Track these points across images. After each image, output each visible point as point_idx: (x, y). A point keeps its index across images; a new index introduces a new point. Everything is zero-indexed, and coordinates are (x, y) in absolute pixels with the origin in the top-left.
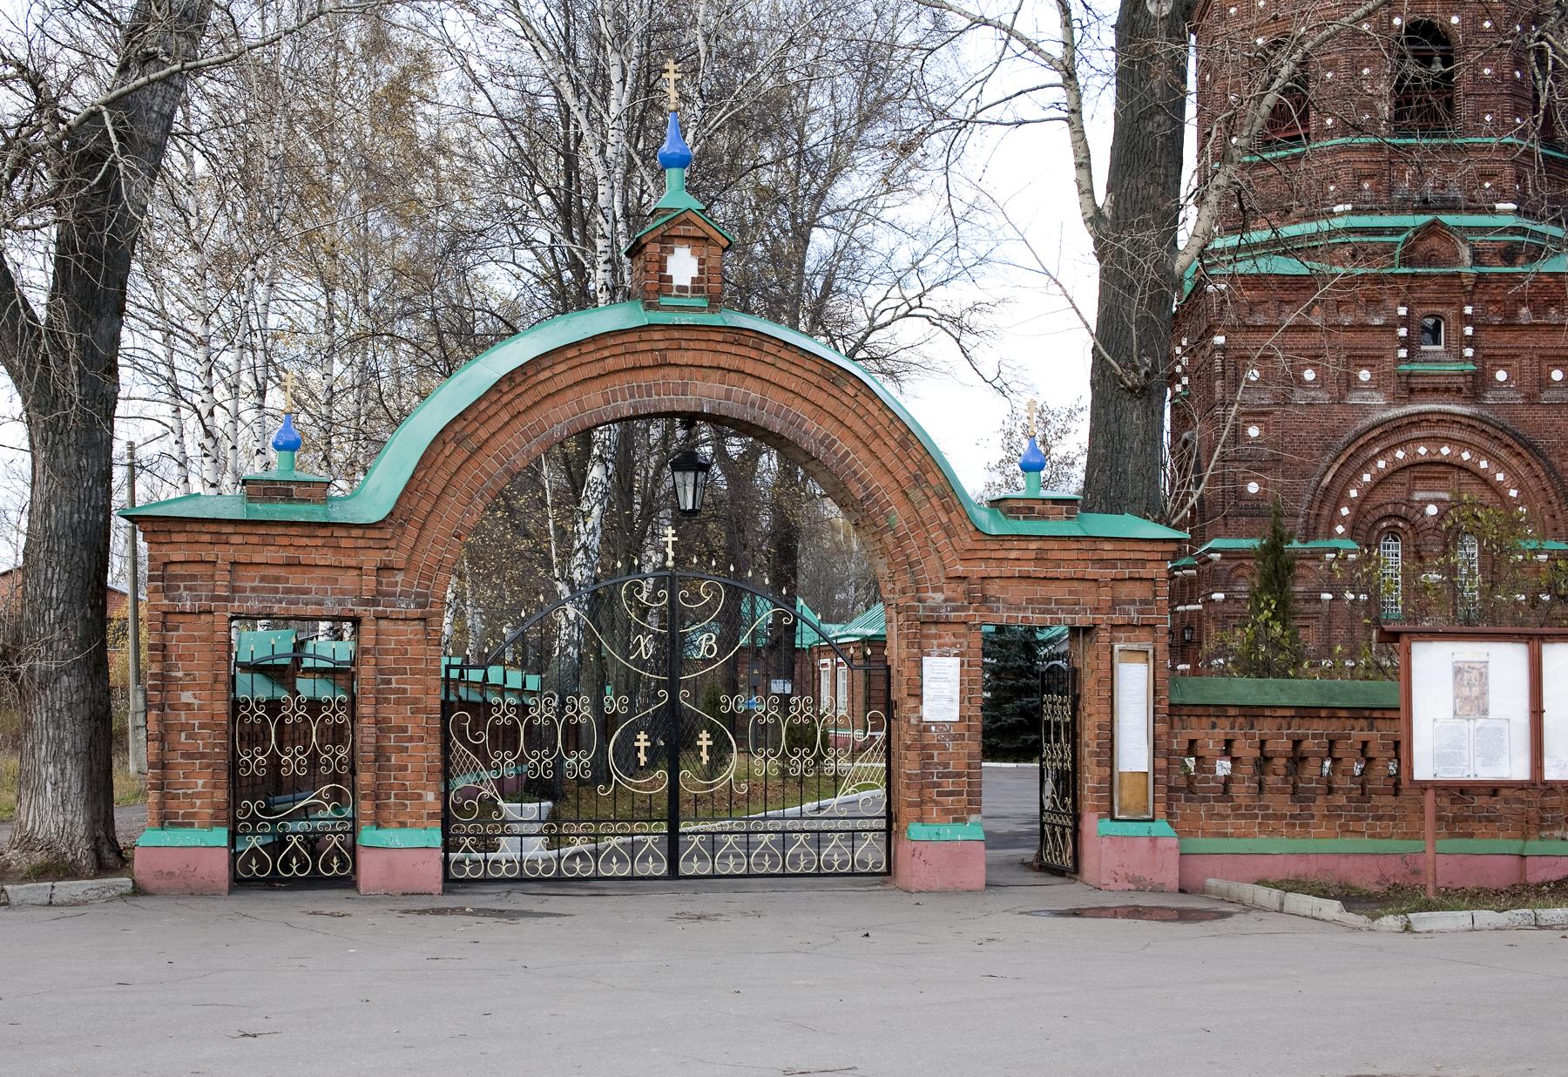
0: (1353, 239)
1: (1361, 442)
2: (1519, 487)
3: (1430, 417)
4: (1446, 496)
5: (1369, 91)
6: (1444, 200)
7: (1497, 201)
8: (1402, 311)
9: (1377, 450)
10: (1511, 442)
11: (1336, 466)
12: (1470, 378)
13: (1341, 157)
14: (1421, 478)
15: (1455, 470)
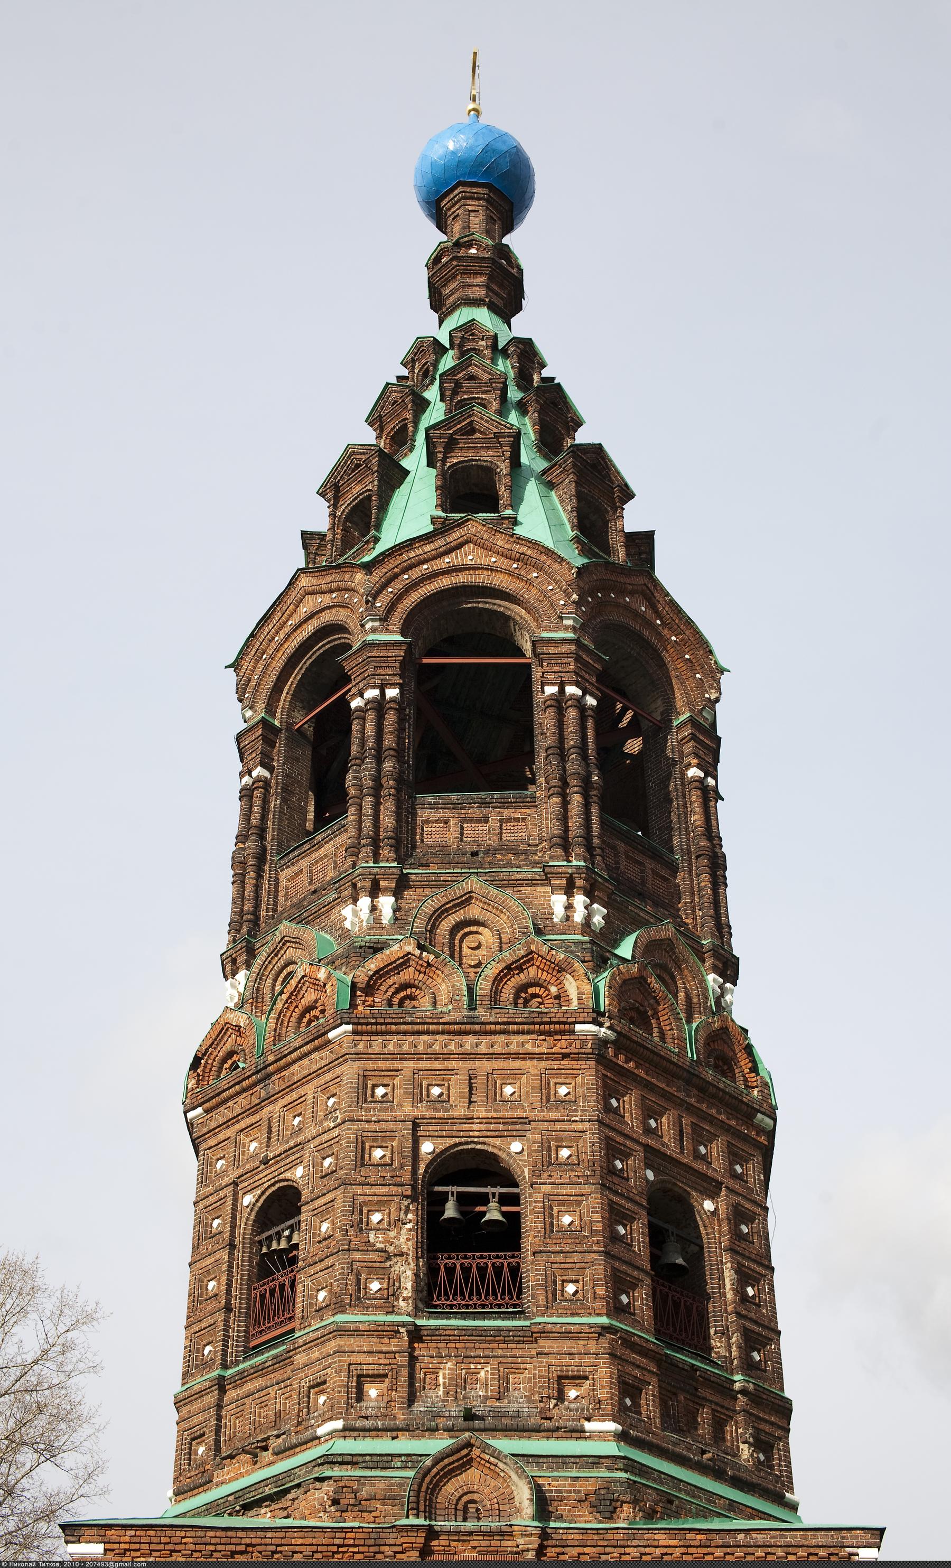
0: (337, 1472)
5: (379, 1246)
6: (500, 1415)
13: (332, 1345)
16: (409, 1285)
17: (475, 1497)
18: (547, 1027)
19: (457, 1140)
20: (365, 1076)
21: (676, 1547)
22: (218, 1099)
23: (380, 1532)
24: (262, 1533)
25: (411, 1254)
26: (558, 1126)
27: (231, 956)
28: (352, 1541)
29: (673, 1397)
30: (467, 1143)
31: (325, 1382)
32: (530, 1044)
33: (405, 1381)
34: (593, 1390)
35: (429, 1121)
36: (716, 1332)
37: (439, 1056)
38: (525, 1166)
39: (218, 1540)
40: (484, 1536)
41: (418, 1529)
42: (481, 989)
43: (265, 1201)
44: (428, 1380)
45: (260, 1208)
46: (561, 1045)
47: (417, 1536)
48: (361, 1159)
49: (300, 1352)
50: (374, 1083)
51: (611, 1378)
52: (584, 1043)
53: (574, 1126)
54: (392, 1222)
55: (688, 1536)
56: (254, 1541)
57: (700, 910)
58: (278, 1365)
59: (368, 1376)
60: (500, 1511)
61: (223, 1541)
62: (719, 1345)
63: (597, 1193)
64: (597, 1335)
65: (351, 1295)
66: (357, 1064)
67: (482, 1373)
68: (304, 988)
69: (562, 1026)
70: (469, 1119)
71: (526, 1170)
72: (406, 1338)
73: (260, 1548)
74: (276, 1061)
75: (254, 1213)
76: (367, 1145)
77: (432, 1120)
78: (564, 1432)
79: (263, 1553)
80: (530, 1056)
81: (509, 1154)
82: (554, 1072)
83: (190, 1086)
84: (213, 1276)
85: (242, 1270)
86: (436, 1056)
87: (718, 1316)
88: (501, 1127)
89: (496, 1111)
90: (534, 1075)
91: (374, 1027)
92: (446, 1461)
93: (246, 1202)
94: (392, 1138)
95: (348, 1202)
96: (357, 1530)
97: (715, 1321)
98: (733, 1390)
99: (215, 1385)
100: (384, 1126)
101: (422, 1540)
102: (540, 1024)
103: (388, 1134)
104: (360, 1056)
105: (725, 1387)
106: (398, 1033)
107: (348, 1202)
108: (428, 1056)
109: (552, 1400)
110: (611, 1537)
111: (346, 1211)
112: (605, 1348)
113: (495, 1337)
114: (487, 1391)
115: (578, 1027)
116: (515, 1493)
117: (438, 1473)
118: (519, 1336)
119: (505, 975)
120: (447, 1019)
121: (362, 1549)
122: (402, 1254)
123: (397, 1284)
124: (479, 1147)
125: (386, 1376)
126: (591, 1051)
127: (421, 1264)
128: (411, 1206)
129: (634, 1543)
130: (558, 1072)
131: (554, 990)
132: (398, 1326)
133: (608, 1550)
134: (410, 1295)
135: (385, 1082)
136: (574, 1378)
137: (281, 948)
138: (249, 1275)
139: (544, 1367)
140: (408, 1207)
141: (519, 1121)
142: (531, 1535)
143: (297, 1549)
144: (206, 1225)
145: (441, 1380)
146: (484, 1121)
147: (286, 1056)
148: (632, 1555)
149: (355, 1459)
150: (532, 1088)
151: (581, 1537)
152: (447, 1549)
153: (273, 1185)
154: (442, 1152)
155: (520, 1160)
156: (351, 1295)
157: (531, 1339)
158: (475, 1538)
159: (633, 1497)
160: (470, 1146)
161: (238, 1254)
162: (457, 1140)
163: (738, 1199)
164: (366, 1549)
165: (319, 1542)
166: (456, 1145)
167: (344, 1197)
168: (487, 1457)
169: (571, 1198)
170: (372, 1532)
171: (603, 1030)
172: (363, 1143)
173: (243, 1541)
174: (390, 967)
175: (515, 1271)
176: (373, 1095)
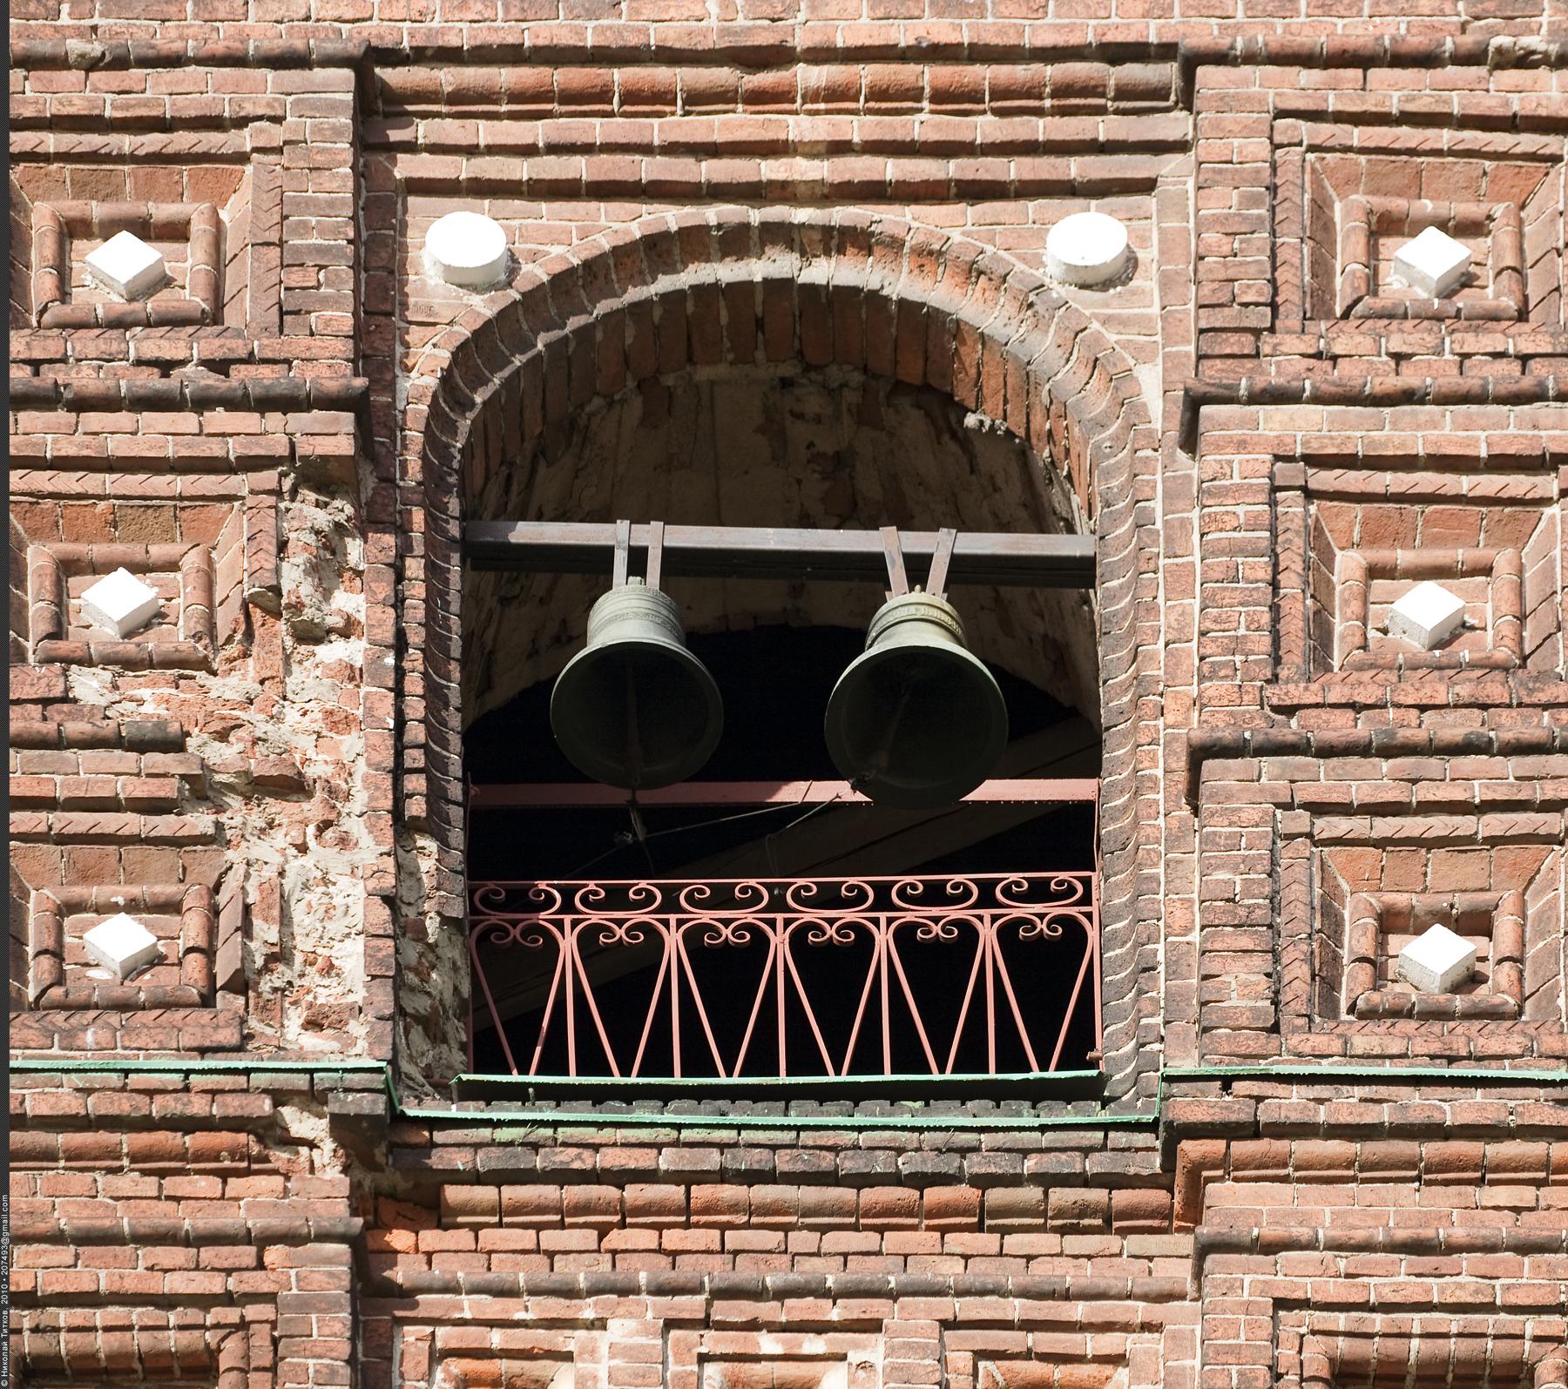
16: (352, 957)
19: (672, 217)
30: (736, 242)
38: (1142, 354)
54: (227, 617)
81: (1030, 300)
88: (985, 127)
118: (1083, 1180)
122: (292, 786)
123: (266, 932)
124: (823, 271)
127: (426, 865)
128: (355, 550)
134: (359, 997)
135: (162, 211)
139: (1248, 1308)
140: (331, 542)
146: (868, 74)
155: (1106, 321)
157: (1157, 1197)
160: (756, 269)
162: (672, 217)
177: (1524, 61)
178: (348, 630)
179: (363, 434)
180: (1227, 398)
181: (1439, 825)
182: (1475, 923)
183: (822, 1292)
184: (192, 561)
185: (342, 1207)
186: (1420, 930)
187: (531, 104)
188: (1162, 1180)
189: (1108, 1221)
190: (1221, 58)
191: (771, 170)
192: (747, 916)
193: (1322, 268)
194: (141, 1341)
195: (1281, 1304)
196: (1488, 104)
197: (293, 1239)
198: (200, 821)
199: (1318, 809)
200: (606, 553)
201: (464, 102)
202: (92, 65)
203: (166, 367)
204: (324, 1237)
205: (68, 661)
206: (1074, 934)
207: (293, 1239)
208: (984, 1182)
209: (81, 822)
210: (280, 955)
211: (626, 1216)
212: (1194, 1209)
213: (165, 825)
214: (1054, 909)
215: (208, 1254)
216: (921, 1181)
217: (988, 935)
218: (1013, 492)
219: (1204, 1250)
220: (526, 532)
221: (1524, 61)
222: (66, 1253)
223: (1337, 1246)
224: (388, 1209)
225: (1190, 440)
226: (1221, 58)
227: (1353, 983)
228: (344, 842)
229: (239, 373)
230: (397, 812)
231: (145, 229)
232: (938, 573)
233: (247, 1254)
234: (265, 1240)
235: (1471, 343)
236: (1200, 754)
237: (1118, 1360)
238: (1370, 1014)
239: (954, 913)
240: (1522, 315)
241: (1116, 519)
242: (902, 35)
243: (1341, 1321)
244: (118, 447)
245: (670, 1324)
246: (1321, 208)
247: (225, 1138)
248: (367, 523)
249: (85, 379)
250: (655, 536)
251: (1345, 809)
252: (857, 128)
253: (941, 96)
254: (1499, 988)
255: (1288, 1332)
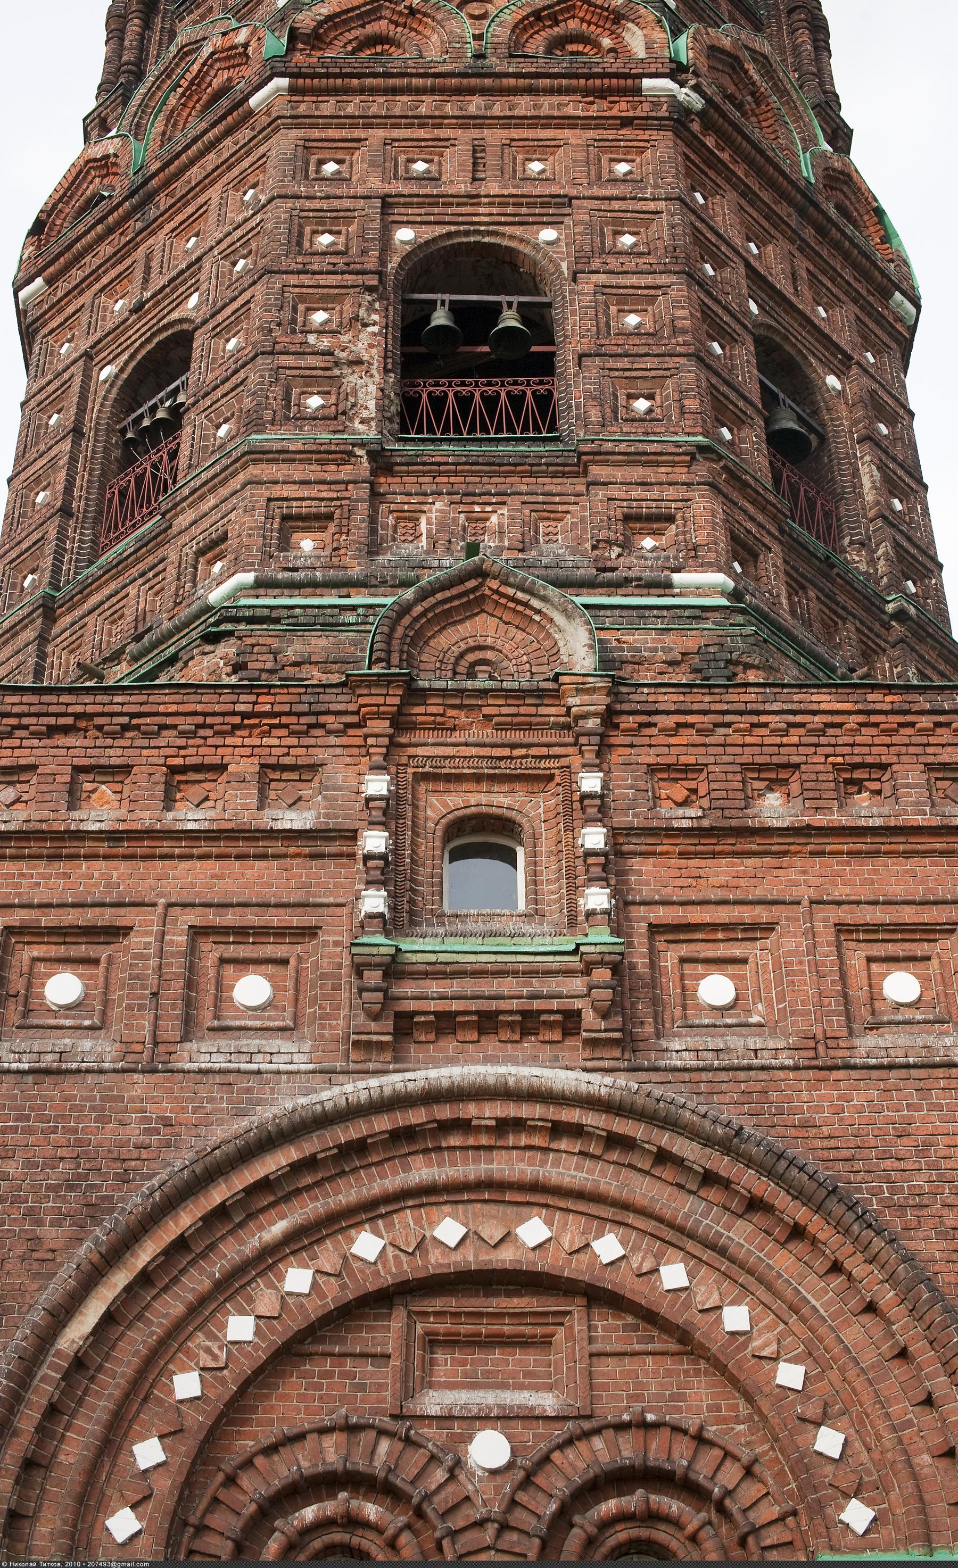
1: (218, 1195)
2: (808, 1356)
3: (470, 1110)
4: (547, 1402)
7: (677, 570)
8: (378, 785)
9: (278, 1228)
10: (764, 1187)
11: (120, 1279)
12: (602, 975)
14: (452, 1342)
15: (576, 1307)
16: (372, 404)
17: (489, 655)
18: (598, 82)
19: (453, 228)
20: (307, 146)
21: (850, 713)
22: (68, 256)
23: (319, 694)
24: (106, 697)
25: (376, 364)
26: (616, 205)
27: (99, 115)
28: (269, 706)
29: (800, 592)
30: (467, 233)
31: (224, 538)
32: (572, 107)
33: (363, 521)
34: (684, 533)
35: (408, 200)
36: (851, 543)
37: (426, 121)
38: (562, 259)
39: (25, 709)
40: (506, 697)
41: (390, 682)
42: (493, 36)
43: (134, 369)
44: (400, 530)
45: (126, 380)
46: (622, 108)
47: (387, 695)
48: (297, 242)
49: (183, 509)
50: (321, 157)
51: (714, 516)
52: (656, 105)
53: (641, 206)
54: (345, 321)
55: (870, 697)
56: (90, 709)
57: (795, 71)
58: (144, 550)
59: (299, 517)
60: (532, 674)
61: (33, 709)
62: (857, 558)
63: (680, 284)
64: (688, 458)
65: (275, 412)
66: (294, 133)
67: (494, 519)
68: (212, 73)
69: (622, 82)
70: (473, 198)
71: (564, 266)
72: (366, 464)
73: (99, 721)
74: (161, 169)
75: (115, 390)
76: (308, 230)
77: (409, 201)
78: (637, 586)
79: (106, 728)
80: (570, 122)
81: (536, 247)
82: (608, 144)
83: (24, 257)
84: (45, 483)
85: (92, 463)
86: (422, 121)
87: (854, 522)
88: (524, 210)
89: (515, 187)
90: (577, 146)
91: (324, 81)
92: (439, 596)
93: (104, 374)
94: (348, 221)
95: (273, 294)
96: (277, 691)
97: (850, 528)
98: (884, 612)
99: (38, 608)
100: (336, 204)
101: (397, 701)
102: (588, 76)
103: (342, 214)
104: (299, 120)
105: (873, 604)
106: (362, 91)
107: (273, 294)
108: (408, 121)
109: (615, 548)
110: (734, 697)
111: (271, 305)
112: (702, 476)
113: (515, 465)
114: (501, 540)
115: (647, 83)
116: (561, 644)
117: (423, 614)
118: (558, 465)
119: (531, 25)
120: (441, 69)
121: (285, 720)
124: (486, 240)
125: (329, 517)
126: (667, 114)
128: (377, 305)
129: (775, 707)
130: (615, 144)
131: (606, 42)
132: (354, 445)
133: (728, 718)
134: (373, 415)
136: (650, 518)
137: (177, 65)
138: (102, 469)
139: (601, 501)
140: (371, 303)
141: (553, 200)
142: (594, 690)
143: (169, 721)
144: (39, 426)
145: (423, 527)
146: (497, 200)
147: (178, 155)
148: (772, 726)
149: (275, 614)
150: (574, 161)
151: (682, 698)
152: (439, 719)
153: (148, 340)
154: (427, 243)
156: (275, 412)
157: (576, 469)
158: (491, 702)
159: (764, 659)
160: (472, 239)
161: (87, 445)
162: (453, 228)
163: (875, 386)
164: (294, 720)
165: (209, 708)
166: (449, 235)
167: (268, 288)
168: (511, 591)
169: (640, 292)
170: (306, 693)
171: (684, 90)
172: (301, 226)
173: (71, 709)
174: (350, 15)
175: (545, 401)
176: (318, 171)
177: (645, 199)
178: (374, 324)
179: (380, 281)
180: (583, 272)
181: (639, 374)
182: (650, 397)
183: (490, 494)
184: (338, 308)
185: (368, 473)
186: (638, 398)
187: (421, 206)
188: (577, 465)
189: (564, 475)
190: (578, 198)
191: (475, 219)
192: (469, 388)
193: (603, 243)
194: (314, 510)
195: (609, 499)
196: (638, 208)
197: (355, 482)
198: (337, 372)
199: (610, 370)
200: (435, 301)
201: (405, 205)
202: (321, 198)
203: (334, 264)
204: (363, 482)
205: (307, 332)
206: (550, 393)
207: (355, 482)
208: (531, 465)
209: (308, 372)
210: (354, 405)
211: (440, 473)
212: (585, 473)
213: (328, 373)
214: (546, 387)
215: (333, 487)
216: (515, 465)
217: (529, 393)
218: (531, 284)
219: (589, 484)
220: (417, 296)
221: (645, 199)
222: (296, 487)
223: (622, 483)
224: (379, 472)
225: (574, 280)
226: (578, 198)
227: (622, 412)
228: (372, 376)
229: (352, 266)
230: (385, 368)
231: (331, 232)
232: (515, 306)
233: (343, 487)
234: (348, 483)
235: (638, 260)
236: (581, 356)
237: (568, 512)
238: (626, 420)
239: (520, 388)
240: (649, 254)
241: (558, 296)
242: (505, 192)
243: (625, 504)
244: (322, 283)
245: (452, 503)
246: (602, 230)
247: (339, 456)
248: (380, 299)
249: (316, 267)
250: (447, 297)
251: (617, 370)
252: (495, 211)
253: (514, 204)
254: (658, 413)
255: (612, 507)
